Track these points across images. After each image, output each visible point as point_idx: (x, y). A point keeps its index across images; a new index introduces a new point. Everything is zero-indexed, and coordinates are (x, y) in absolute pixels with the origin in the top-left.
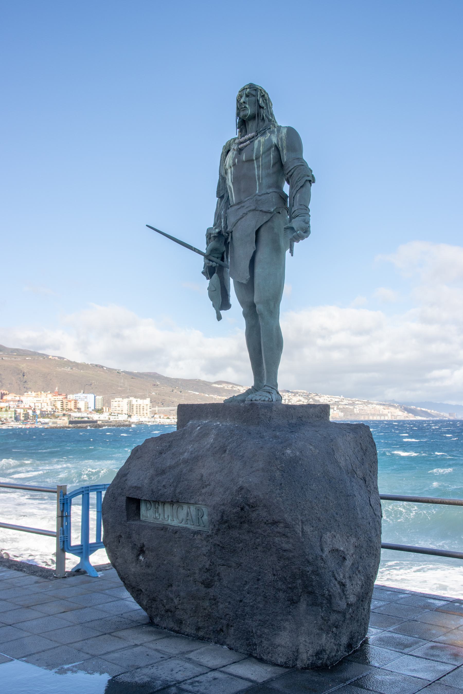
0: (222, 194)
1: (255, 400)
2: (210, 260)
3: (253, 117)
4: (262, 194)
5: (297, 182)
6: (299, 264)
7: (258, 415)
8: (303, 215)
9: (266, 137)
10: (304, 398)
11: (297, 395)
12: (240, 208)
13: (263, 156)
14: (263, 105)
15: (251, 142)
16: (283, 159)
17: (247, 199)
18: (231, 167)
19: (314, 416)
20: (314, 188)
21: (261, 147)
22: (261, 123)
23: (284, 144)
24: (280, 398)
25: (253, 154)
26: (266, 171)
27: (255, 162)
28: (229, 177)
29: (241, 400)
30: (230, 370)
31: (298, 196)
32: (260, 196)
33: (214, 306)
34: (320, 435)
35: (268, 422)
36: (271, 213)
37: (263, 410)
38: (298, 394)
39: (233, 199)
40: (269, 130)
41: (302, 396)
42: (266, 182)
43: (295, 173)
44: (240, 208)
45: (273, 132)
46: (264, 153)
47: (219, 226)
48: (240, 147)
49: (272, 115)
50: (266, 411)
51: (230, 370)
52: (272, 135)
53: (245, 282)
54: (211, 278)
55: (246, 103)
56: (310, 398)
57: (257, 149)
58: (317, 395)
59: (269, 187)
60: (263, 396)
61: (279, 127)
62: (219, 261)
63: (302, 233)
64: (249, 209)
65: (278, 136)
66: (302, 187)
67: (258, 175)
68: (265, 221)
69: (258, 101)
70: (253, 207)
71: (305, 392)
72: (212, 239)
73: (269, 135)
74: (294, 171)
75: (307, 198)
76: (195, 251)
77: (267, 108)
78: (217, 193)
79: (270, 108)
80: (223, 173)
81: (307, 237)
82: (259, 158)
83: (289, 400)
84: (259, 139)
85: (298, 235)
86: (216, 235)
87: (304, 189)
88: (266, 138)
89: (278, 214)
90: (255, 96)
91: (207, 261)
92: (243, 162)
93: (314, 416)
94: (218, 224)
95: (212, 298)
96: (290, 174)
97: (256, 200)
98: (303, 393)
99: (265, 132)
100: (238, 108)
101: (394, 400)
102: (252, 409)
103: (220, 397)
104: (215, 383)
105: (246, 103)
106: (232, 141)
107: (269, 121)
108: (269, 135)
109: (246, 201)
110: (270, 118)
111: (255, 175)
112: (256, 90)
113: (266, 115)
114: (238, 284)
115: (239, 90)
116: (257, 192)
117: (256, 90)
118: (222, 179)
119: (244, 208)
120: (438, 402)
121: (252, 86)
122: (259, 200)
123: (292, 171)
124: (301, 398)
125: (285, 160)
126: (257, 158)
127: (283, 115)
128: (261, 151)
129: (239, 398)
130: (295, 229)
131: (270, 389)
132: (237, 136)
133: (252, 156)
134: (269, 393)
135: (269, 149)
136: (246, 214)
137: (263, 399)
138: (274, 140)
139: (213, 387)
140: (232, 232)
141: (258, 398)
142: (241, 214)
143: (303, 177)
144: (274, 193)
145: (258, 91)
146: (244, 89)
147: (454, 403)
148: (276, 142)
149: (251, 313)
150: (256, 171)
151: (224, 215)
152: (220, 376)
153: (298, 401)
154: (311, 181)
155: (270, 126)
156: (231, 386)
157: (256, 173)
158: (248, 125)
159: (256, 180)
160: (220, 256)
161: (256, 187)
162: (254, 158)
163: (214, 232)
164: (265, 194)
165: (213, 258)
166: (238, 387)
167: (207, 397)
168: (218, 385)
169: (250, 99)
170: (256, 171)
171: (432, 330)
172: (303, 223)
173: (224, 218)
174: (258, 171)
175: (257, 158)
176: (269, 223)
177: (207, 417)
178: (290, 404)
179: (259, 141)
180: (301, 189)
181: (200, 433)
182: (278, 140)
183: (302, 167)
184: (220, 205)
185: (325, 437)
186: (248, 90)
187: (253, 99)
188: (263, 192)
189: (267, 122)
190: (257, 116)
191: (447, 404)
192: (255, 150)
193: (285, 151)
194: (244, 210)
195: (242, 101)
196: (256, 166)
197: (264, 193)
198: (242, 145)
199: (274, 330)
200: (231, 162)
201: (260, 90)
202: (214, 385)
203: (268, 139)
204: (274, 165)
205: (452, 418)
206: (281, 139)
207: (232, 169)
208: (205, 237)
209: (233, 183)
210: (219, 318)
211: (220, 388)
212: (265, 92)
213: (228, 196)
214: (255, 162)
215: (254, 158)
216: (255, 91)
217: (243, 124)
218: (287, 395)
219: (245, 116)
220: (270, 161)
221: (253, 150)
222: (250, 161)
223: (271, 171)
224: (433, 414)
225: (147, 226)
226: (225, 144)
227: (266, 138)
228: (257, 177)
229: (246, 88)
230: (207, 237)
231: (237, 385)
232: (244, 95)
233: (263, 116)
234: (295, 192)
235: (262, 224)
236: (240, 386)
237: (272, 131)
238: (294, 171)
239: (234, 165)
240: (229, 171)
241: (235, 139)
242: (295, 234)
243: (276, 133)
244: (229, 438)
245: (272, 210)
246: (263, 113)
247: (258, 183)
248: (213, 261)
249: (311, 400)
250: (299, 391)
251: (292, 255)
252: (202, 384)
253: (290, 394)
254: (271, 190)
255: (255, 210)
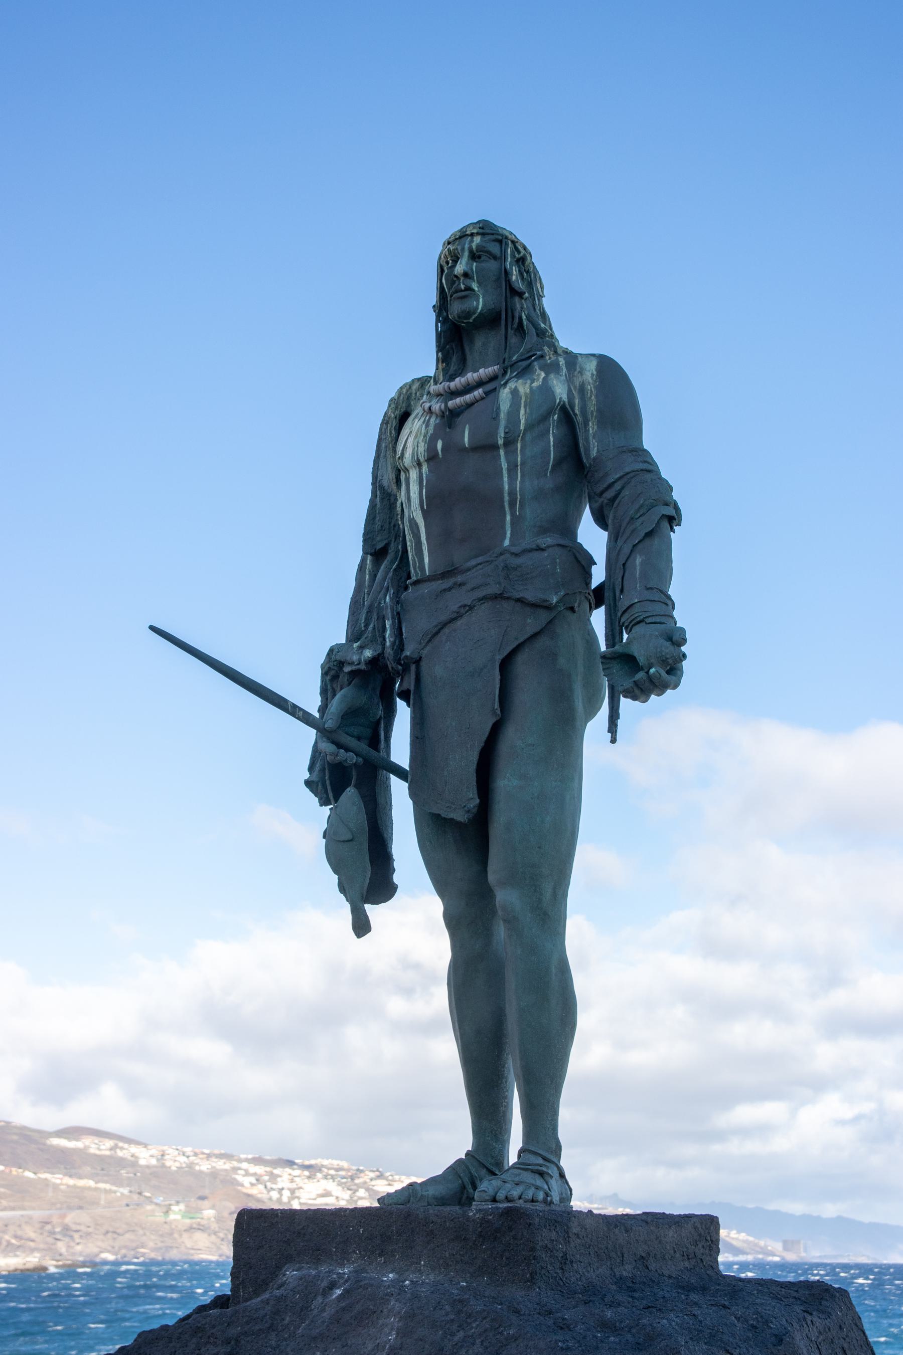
0: (384, 540)
1: (508, 1199)
2: (339, 746)
3: (491, 320)
4: (525, 551)
5: (632, 518)
6: (630, 766)
7: (533, 1249)
8: (658, 619)
9: (533, 381)
10: (340, 1184)
11: (319, 1175)
12: (450, 589)
13: (528, 437)
14: (520, 285)
15: (487, 393)
16: (587, 450)
17: (473, 562)
18: (419, 464)
19: (678, 1255)
20: (678, 537)
21: (522, 411)
22: (513, 340)
23: (592, 406)
24: (567, 1194)
25: (497, 428)
26: (536, 482)
27: (502, 452)
28: (412, 497)
29: (435, 1198)
30: (110, 1091)
31: (638, 560)
32: (516, 555)
33: (342, 889)
34: (738, 1319)
35: (559, 1271)
36: (547, 607)
37: (545, 1233)
38: (320, 1171)
39: (424, 559)
40: (541, 361)
41: (333, 1178)
42: (532, 513)
43: (626, 492)
44: (450, 589)
45: (553, 368)
46: (529, 427)
47: (373, 640)
48: (451, 404)
49: (544, 316)
50: (554, 1235)
51: (110, 1091)
52: (552, 376)
53: (460, 816)
54: (336, 799)
55: (472, 278)
56: (359, 1186)
57: (509, 413)
58: (381, 1176)
59: (543, 531)
60: (529, 1186)
61: (572, 359)
62: (363, 747)
63: (663, 673)
64: (480, 593)
65: (570, 380)
66: (649, 534)
67: (512, 493)
68: (530, 631)
69: (507, 273)
70: (494, 589)
71: (345, 1164)
72: (344, 679)
73: (543, 375)
74: (623, 488)
75: (661, 569)
76: (293, 714)
77: (532, 295)
78: (365, 541)
79: (540, 297)
80: (388, 477)
81: (675, 687)
82: (514, 441)
83: (292, 1191)
84: (512, 385)
85: (650, 679)
86: (363, 667)
87: (656, 541)
88: (535, 384)
89: (568, 614)
90: (501, 258)
91: (327, 747)
92: (464, 450)
93: (678, 1255)
94: (369, 633)
95: (336, 861)
96: (610, 494)
97: (506, 567)
98: (337, 1170)
99: (530, 364)
100: (441, 290)
101: (615, 1195)
102: (510, 1229)
103: (71, 1182)
104: (60, 1133)
105: (472, 278)
106: (415, 387)
107: (538, 335)
108: (543, 375)
109: (469, 570)
110: (543, 325)
111: (501, 490)
112: (500, 242)
113: (528, 317)
114: (433, 826)
115: (447, 236)
116: (507, 543)
117: (500, 242)
118: (382, 499)
119: (464, 588)
120: (751, 1206)
121: (486, 229)
122: (515, 569)
123: (617, 486)
124: (331, 1186)
125: (594, 453)
126: (509, 443)
127: (578, 319)
128: (523, 421)
129: (431, 1191)
130: (641, 660)
131: (541, 1161)
132: (432, 374)
133: (495, 434)
134: (541, 1174)
135: (545, 418)
136: (471, 608)
137: (530, 1194)
138: (560, 391)
139: (52, 1146)
140: (418, 661)
141: (515, 1193)
142: (455, 608)
143: (653, 506)
144: (558, 551)
145: (507, 245)
146: (462, 235)
147: (796, 1208)
148: (565, 398)
149: (471, 917)
150: (505, 479)
151: (392, 609)
152: (79, 1113)
153: (322, 1196)
154: (673, 520)
155: (542, 350)
156: (109, 1143)
157: (506, 487)
158: (472, 342)
159: (503, 507)
160: (368, 732)
161: (503, 528)
162: (501, 442)
163: (355, 658)
164: (531, 550)
165: (349, 738)
166: (134, 1149)
167: (29, 1180)
168: (69, 1139)
169: (484, 265)
170: (505, 479)
171: (735, 978)
172: (668, 644)
173: (393, 618)
174: (512, 479)
175: (509, 443)
176: (543, 642)
177: (344, 1258)
178: (296, 1205)
179: (515, 393)
180: (647, 542)
181: (343, 1309)
182: (570, 392)
183: (648, 476)
184: (374, 576)
185: (753, 1326)
186: (477, 239)
187: (492, 265)
188: (527, 542)
189: (531, 337)
190: (503, 317)
191: (777, 1213)
192: (503, 416)
193: (592, 428)
194: (463, 597)
195: (460, 268)
196: (504, 466)
197: (529, 547)
198: (459, 401)
199: (554, 970)
200: (422, 448)
201: (513, 242)
202: (56, 1141)
203: (540, 388)
204: (558, 464)
205: (791, 1257)
206: (582, 390)
207: (425, 469)
208: (318, 673)
209: (426, 514)
210: (361, 926)
211: (75, 1151)
212: (525, 248)
213: (405, 551)
214: (502, 452)
215: (501, 442)
216: (497, 244)
217: (456, 336)
218: (286, 1177)
219: (468, 314)
220: (546, 452)
221: (496, 418)
222: (486, 448)
223: (548, 483)
224: (734, 1243)
225: (152, 628)
226: (393, 394)
227: (535, 384)
228: (507, 498)
229: (472, 235)
230: (325, 674)
231: (130, 1141)
232: (466, 254)
233: (520, 318)
234: (626, 550)
235: (521, 640)
236: (138, 1143)
237: (551, 364)
238: (623, 488)
239: (432, 457)
240: (413, 475)
241: (423, 382)
242: (641, 675)
243: (564, 370)
244: (455, 1327)
245: (555, 601)
246: (521, 308)
247: (508, 518)
248: (347, 750)
249: (362, 1193)
250: (326, 1162)
251: (613, 741)
252: (15, 1137)
253: (297, 1172)
254: (548, 540)
255: (498, 597)
